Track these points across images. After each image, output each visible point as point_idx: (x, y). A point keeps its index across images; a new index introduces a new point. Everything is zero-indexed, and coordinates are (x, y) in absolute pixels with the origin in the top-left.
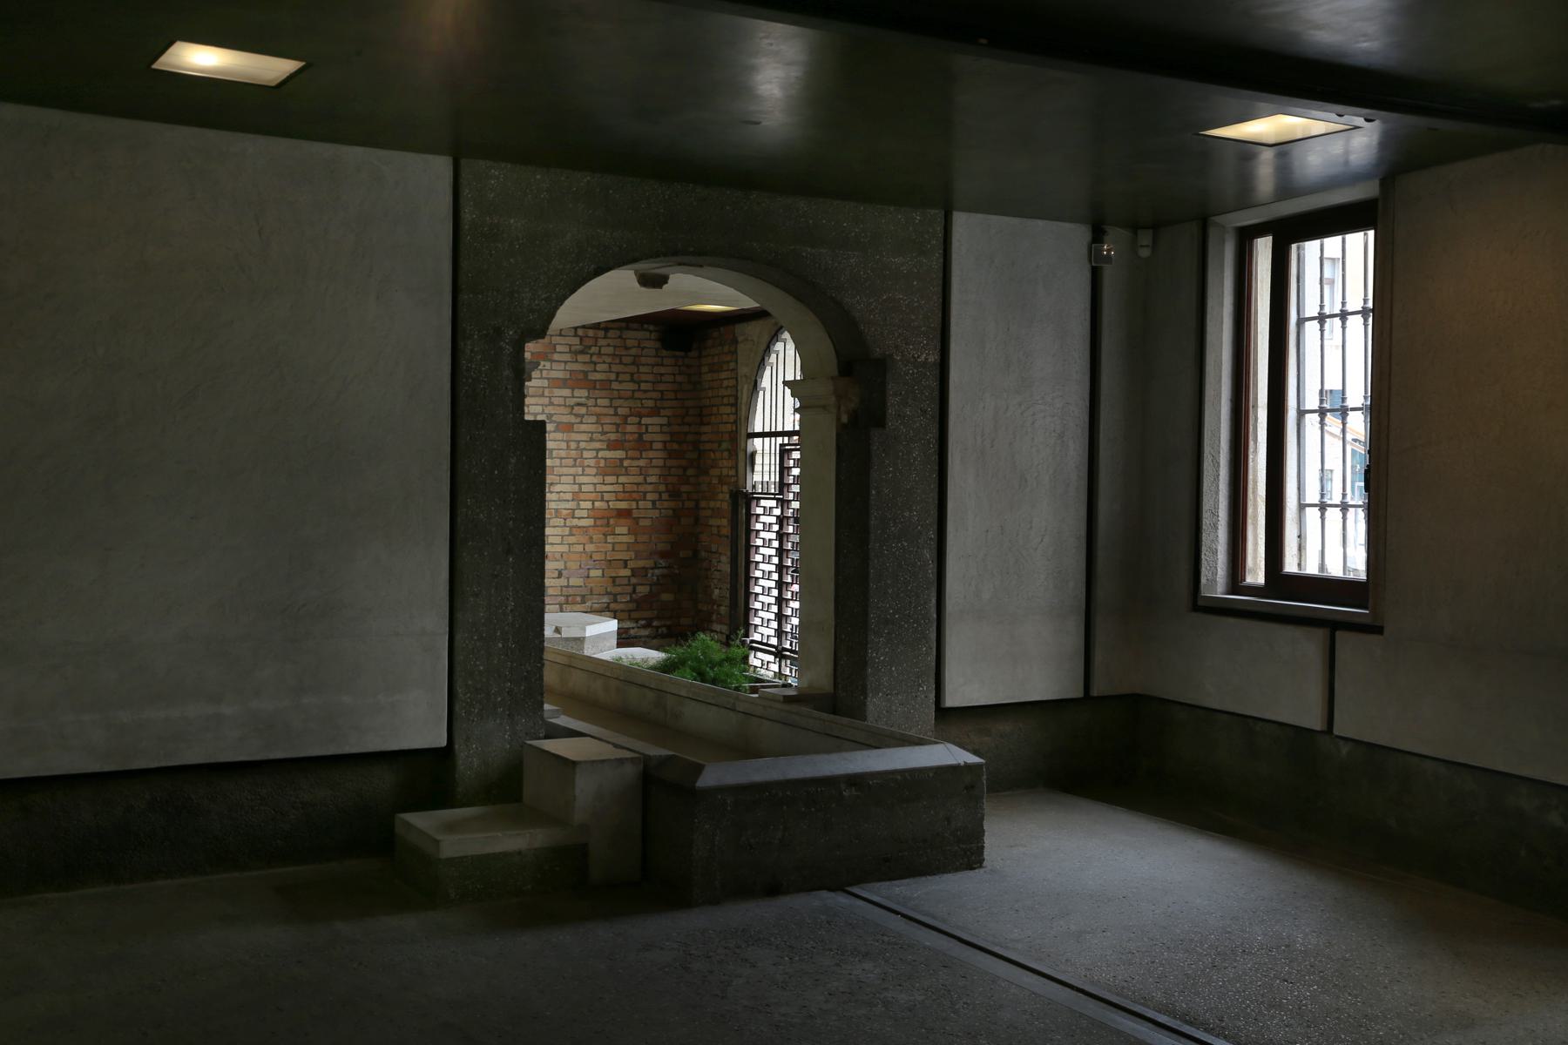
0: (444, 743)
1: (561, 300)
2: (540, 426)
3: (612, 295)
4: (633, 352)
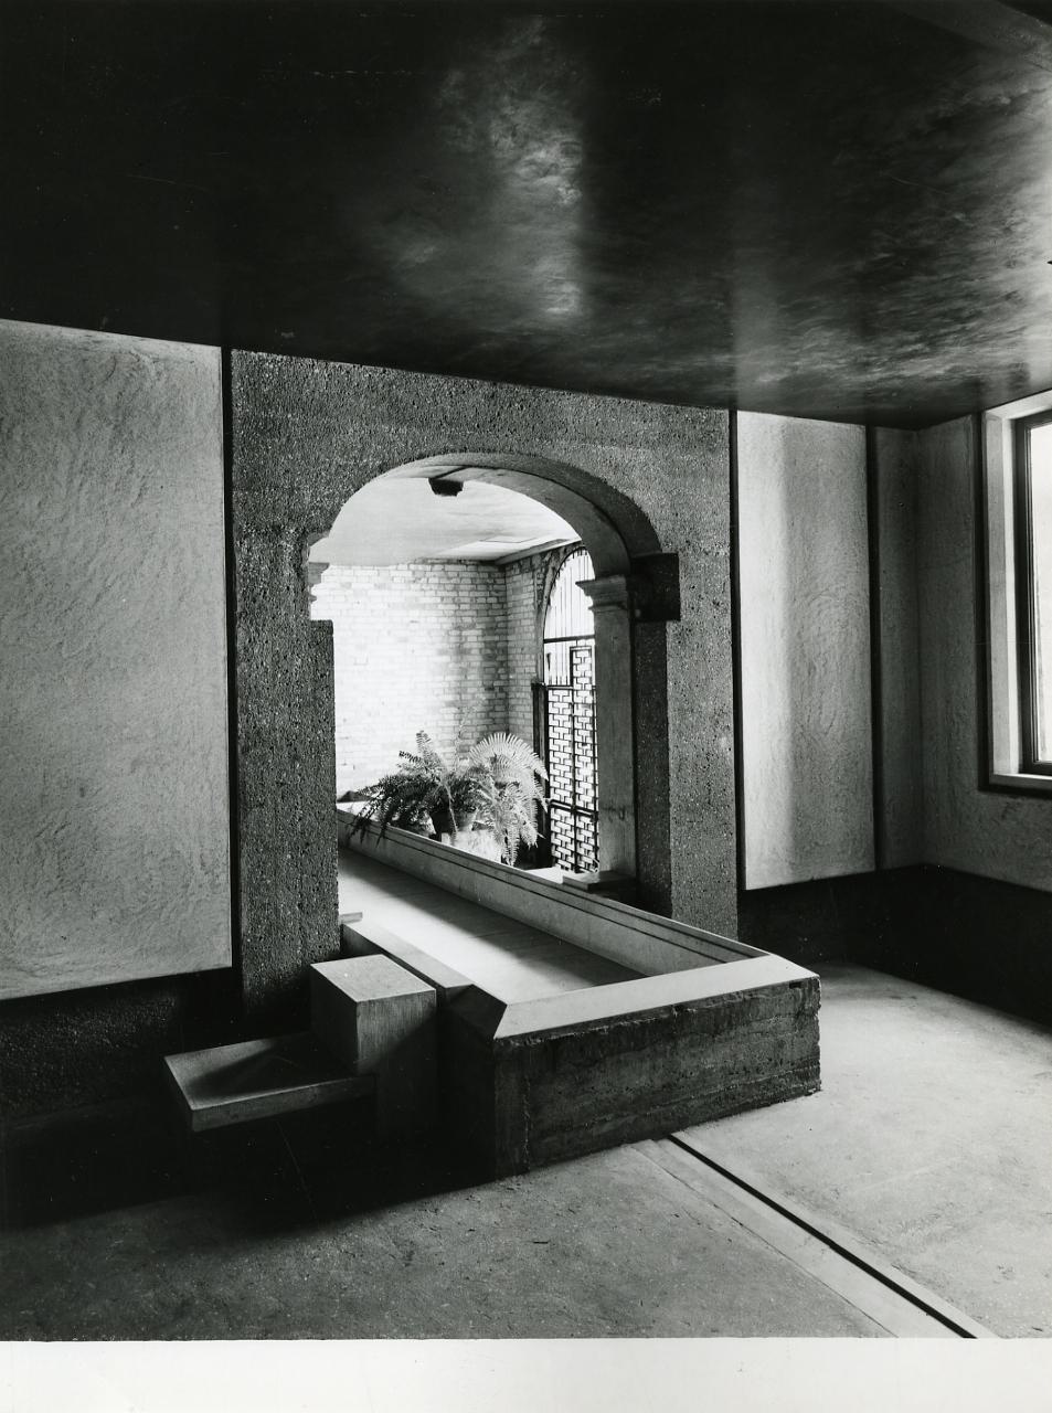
0: (229, 963)
1: (347, 496)
2: (326, 628)
4: (453, 581)
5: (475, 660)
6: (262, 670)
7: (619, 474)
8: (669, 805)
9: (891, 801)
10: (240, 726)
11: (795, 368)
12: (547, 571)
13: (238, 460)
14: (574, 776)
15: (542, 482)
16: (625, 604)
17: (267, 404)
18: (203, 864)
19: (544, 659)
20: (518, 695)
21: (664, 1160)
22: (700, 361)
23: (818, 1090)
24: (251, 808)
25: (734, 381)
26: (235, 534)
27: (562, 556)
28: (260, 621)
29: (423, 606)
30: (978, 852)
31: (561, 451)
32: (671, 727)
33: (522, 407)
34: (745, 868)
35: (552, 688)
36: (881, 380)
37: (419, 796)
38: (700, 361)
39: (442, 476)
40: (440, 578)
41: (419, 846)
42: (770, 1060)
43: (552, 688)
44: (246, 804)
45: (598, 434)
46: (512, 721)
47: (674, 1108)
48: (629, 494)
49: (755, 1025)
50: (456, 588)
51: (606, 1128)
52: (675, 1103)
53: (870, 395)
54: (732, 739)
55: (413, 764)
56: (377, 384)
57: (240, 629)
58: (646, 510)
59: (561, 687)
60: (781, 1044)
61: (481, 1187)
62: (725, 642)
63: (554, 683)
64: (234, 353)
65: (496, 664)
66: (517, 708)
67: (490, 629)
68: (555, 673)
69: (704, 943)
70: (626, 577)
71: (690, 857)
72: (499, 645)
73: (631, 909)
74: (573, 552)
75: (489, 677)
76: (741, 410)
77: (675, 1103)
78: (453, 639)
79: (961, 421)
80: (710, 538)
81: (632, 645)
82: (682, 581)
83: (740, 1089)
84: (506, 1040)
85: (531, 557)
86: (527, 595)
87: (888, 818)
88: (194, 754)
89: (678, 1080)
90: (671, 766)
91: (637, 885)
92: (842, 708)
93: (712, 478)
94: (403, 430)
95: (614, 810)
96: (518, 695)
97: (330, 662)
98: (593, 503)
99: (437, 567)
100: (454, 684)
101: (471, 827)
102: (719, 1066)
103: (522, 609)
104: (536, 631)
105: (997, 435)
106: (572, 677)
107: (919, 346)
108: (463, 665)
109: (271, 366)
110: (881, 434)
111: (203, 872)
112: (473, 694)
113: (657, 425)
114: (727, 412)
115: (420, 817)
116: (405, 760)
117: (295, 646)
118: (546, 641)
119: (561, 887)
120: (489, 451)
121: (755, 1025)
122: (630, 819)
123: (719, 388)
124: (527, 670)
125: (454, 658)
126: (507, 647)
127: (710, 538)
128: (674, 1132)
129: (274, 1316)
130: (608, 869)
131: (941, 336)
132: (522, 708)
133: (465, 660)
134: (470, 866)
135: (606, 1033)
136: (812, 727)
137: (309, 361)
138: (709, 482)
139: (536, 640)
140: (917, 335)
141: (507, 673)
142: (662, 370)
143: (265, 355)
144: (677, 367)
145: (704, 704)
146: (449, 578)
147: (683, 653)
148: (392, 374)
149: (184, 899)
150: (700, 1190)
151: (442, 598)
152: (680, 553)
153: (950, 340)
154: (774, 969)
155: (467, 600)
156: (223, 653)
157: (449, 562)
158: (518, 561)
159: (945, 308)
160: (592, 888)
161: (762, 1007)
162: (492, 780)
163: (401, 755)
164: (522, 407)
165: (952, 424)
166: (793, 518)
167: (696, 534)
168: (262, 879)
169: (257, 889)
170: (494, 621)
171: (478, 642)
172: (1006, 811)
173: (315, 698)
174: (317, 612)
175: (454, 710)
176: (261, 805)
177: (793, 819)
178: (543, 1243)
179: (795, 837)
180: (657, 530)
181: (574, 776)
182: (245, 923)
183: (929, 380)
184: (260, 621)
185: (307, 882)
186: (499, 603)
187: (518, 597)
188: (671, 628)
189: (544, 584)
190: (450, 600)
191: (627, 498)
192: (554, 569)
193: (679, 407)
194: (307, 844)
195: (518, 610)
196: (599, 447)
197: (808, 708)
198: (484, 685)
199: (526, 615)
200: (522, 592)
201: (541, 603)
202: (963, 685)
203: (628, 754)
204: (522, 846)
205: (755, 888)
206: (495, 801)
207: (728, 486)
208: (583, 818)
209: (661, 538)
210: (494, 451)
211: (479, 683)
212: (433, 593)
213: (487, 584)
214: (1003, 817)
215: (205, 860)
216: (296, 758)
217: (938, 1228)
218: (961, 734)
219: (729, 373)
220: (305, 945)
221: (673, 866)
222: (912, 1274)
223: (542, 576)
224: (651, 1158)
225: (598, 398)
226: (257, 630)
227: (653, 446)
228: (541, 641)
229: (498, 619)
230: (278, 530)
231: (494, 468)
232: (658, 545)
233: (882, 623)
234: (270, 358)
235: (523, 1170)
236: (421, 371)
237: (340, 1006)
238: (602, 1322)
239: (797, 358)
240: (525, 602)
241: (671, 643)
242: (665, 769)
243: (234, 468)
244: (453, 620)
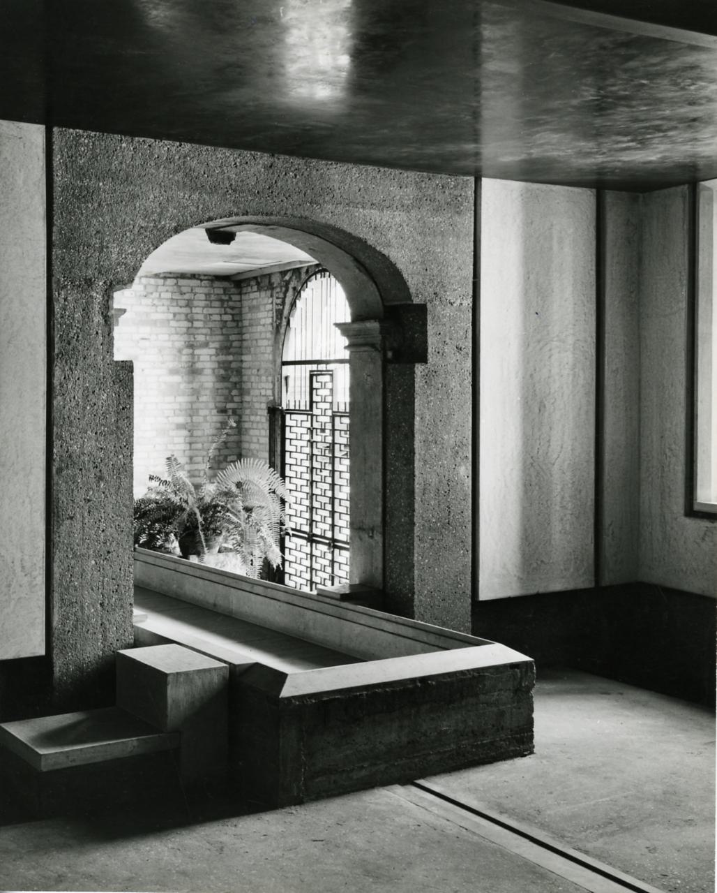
0: (42, 652)
1: (147, 254)
2: (128, 367)
3: (190, 250)
4: (187, 296)
5: (208, 380)
6: (74, 404)
7: (378, 234)
8: (414, 524)
9: (610, 525)
10: (55, 450)
11: (531, 154)
12: (287, 290)
13: (58, 222)
14: (312, 503)
15: (308, 236)
16: (378, 346)
17: (82, 174)
18: (23, 567)
19: (280, 382)
20: (252, 418)
21: (409, 796)
22: (451, 148)
23: (532, 753)
24: (63, 520)
25: (480, 159)
26: (54, 286)
27: (304, 276)
28: (73, 361)
29: (154, 323)
30: (682, 570)
31: (327, 214)
32: (417, 456)
33: (296, 175)
34: (478, 581)
35: (291, 412)
36: (603, 162)
37: (166, 520)
38: (451, 148)
39: (219, 228)
40: (172, 293)
41: (172, 565)
42: (493, 726)
43: (291, 412)
44: (59, 517)
45: (360, 199)
46: (245, 445)
47: (417, 760)
48: (385, 252)
49: (482, 697)
50: (189, 304)
51: (363, 773)
52: (417, 757)
53: (601, 171)
54: (470, 468)
55: (162, 488)
56: (173, 156)
57: (57, 368)
58: (400, 266)
59: (299, 412)
60: (501, 714)
61: (268, 813)
62: (466, 382)
63: (292, 407)
64: (55, 130)
65: (229, 385)
66: (252, 432)
67: (225, 348)
68: (294, 396)
69: (442, 638)
70: (381, 321)
71: (431, 573)
72: (233, 365)
73: (380, 614)
74: (315, 273)
75: (222, 399)
76: (485, 177)
77: (417, 757)
78: (184, 358)
79: (680, 189)
80: (455, 290)
81: (384, 384)
82: (429, 328)
83: (469, 748)
84: (289, 699)
85: (270, 275)
86: (265, 314)
87: (607, 540)
88: (17, 474)
89: (420, 738)
90: (417, 491)
91: (384, 592)
92: (568, 439)
93: (458, 237)
94: (195, 196)
95: (364, 530)
96: (252, 418)
97: (131, 396)
98: (352, 255)
99: (169, 282)
100: (184, 406)
101: (217, 549)
102: (452, 729)
103: (260, 328)
104: (274, 353)
105: (708, 204)
106: (312, 402)
107: (631, 144)
108: (195, 385)
109: (86, 141)
110: (610, 197)
111: (23, 574)
112: (205, 416)
113: (411, 191)
114: (472, 179)
115: (167, 540)
116: (155, 484)
117: (101, 383)
118: (285, 363)
119: (316, 598)
120: (267, 214)
121: (482, 697)
122: (378, 538)
123: (469, 163)
124: (263, 392)
125: (186, 378)
126: (241, 368)
127: (455, 290)
128: (416, 779)
129: (130, 879)
130: (357, 583)
131: (648, 139)
132: (257, 432)
133: (197, 380)
134: (226, 583)
135: (365, 697)
136: (541, 459)
137: (118, 137)
138: (455, 239)
139: (274, 361)
140: (629, 138)
141: (241, 395)
142: (419, 152)
143: (81, 131)
144: (431, 150)
145: (446, 437)
146: (182, 294)
147: (429, 392)
148: (187, 147)
149: (7, 597)
150: (436, 812)
151: (175, 315)
152: (428, 304)
153: (656, 141)
154: (497, 654)
155: (201, 317)
156: (43, 388)
157: (183, 276)
158: (255, 278)
159: (647, 125)
160: (344, 597)
161: (487, 683)
162: (240, 503)
163: (151, 478)
164: (296, 175)
165: (672, 190)
166: (528, 273)
167: (443, 287)
168: (71, 581)
169: (67, 589)
170: (228, 340)
171: (211, 361)
172: (705, 534)
173: (117, 428)
174: (119, 356)
175: (185, 433)
176: (71, 518)
177: (522, 539)
178: (320, 841)
179: (524, 555)
180: (409, 284)
181: (312, 503)
182: (56, 618)
183: (645, 163)
184: (73, 361)
185: (108, 584)
186: (233, 320)
187: (254, 316)
188: (419, 369)
189: (283, 303)
190: (183, 317)
191: (384, 255)
192: (294, 289)
193: (431, 175)
194: (109, 552)
195: (254, 329)
196: (361, 210)
197: (538, 442)
198: (216, 407)
199: (263, 336)
200: (259, 311)
201: (280, 323)
202: (674, 423)
203: (377, 479)
204: (267, 563)
205: (484, 599)
206: (243, 525)
207: (472, 244)
208: (320, 546)
209: (412, 291)
210: (272, 214)
211: (212, 405)
212: (165, 308)
213: (222, 301)
214: (703, 539)
215: (25, 564)
216: (100, 478)
217: (609, 829)
218: (671, 466)
219: (477, 155)
220: (105, 638)
221: (416, 577)
222: (586, 852)
223: (281, 295)
224: (398, 795)
225: (361, 167)
226: (71, 369)
227: (407, 209)
228: (279, 362)
229: (232, 338)
230: (89, 283)
231: (267, 225)
232: (409, 296)
233: (606, 367)
234: (85, 134)
235: (299, 802)
236: (211, 145)
237: (155, 679)
238: (367, 878)
239: (531, 148)
240: (263, 322)
241: (419, 382)
242: (411, 492)
243: (55, 229)
244: (185, 338)
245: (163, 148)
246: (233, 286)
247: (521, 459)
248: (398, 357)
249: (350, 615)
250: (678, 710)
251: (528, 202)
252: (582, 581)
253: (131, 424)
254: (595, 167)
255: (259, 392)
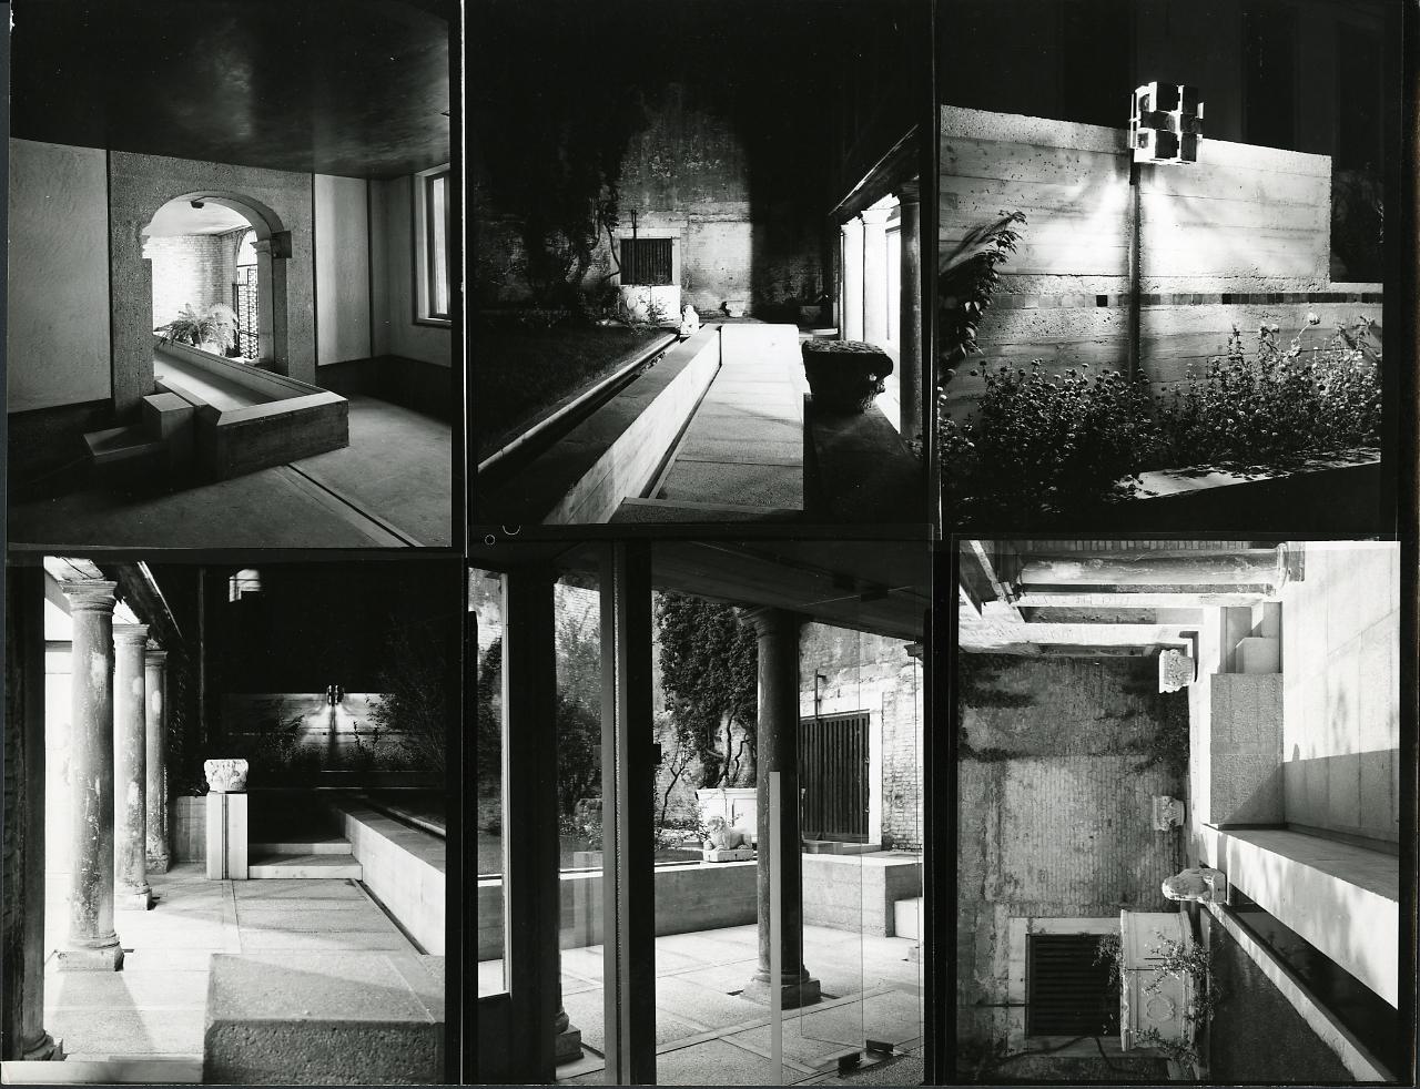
2: (149, 262)
5: (209, 274)
13: (113, 194)
31: (243, 190)
67: (216, 262)
68: (242, 279)
71: (295, 354)
87: (376, 336)
91: (274, 364)
92: (357, 291)
97: (151, 275)
122: (271, 337)
160: (256, 365)
174: (145, 256)
217: (396, 500)
235: (228, 478)
245: (163, 160)
246: (218, 237)
247: (77, 846)
248: (279, 256)
249: (258, 374)
250: (417, 418)
251: (336, 184)
252: (366, 355)
253: (151, 286)
254: (193, 832)
255: (229, 278)
